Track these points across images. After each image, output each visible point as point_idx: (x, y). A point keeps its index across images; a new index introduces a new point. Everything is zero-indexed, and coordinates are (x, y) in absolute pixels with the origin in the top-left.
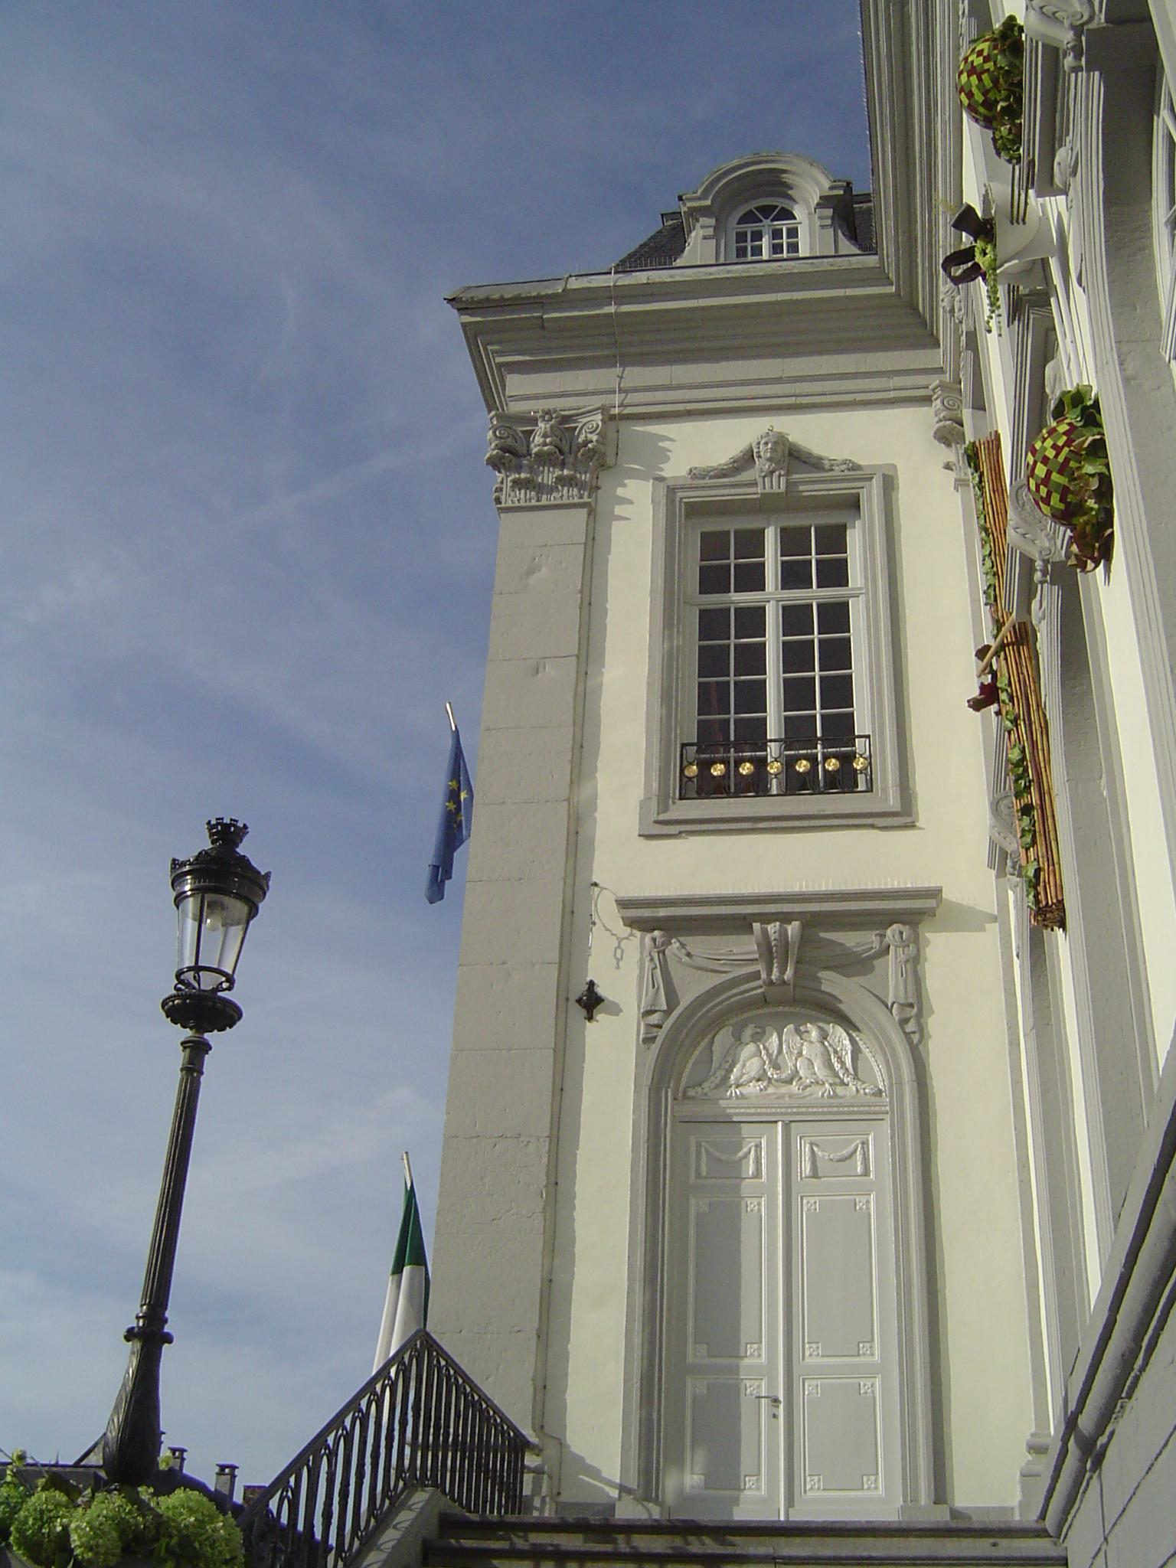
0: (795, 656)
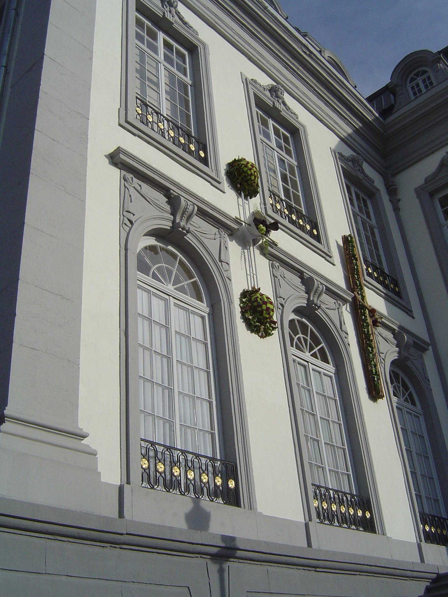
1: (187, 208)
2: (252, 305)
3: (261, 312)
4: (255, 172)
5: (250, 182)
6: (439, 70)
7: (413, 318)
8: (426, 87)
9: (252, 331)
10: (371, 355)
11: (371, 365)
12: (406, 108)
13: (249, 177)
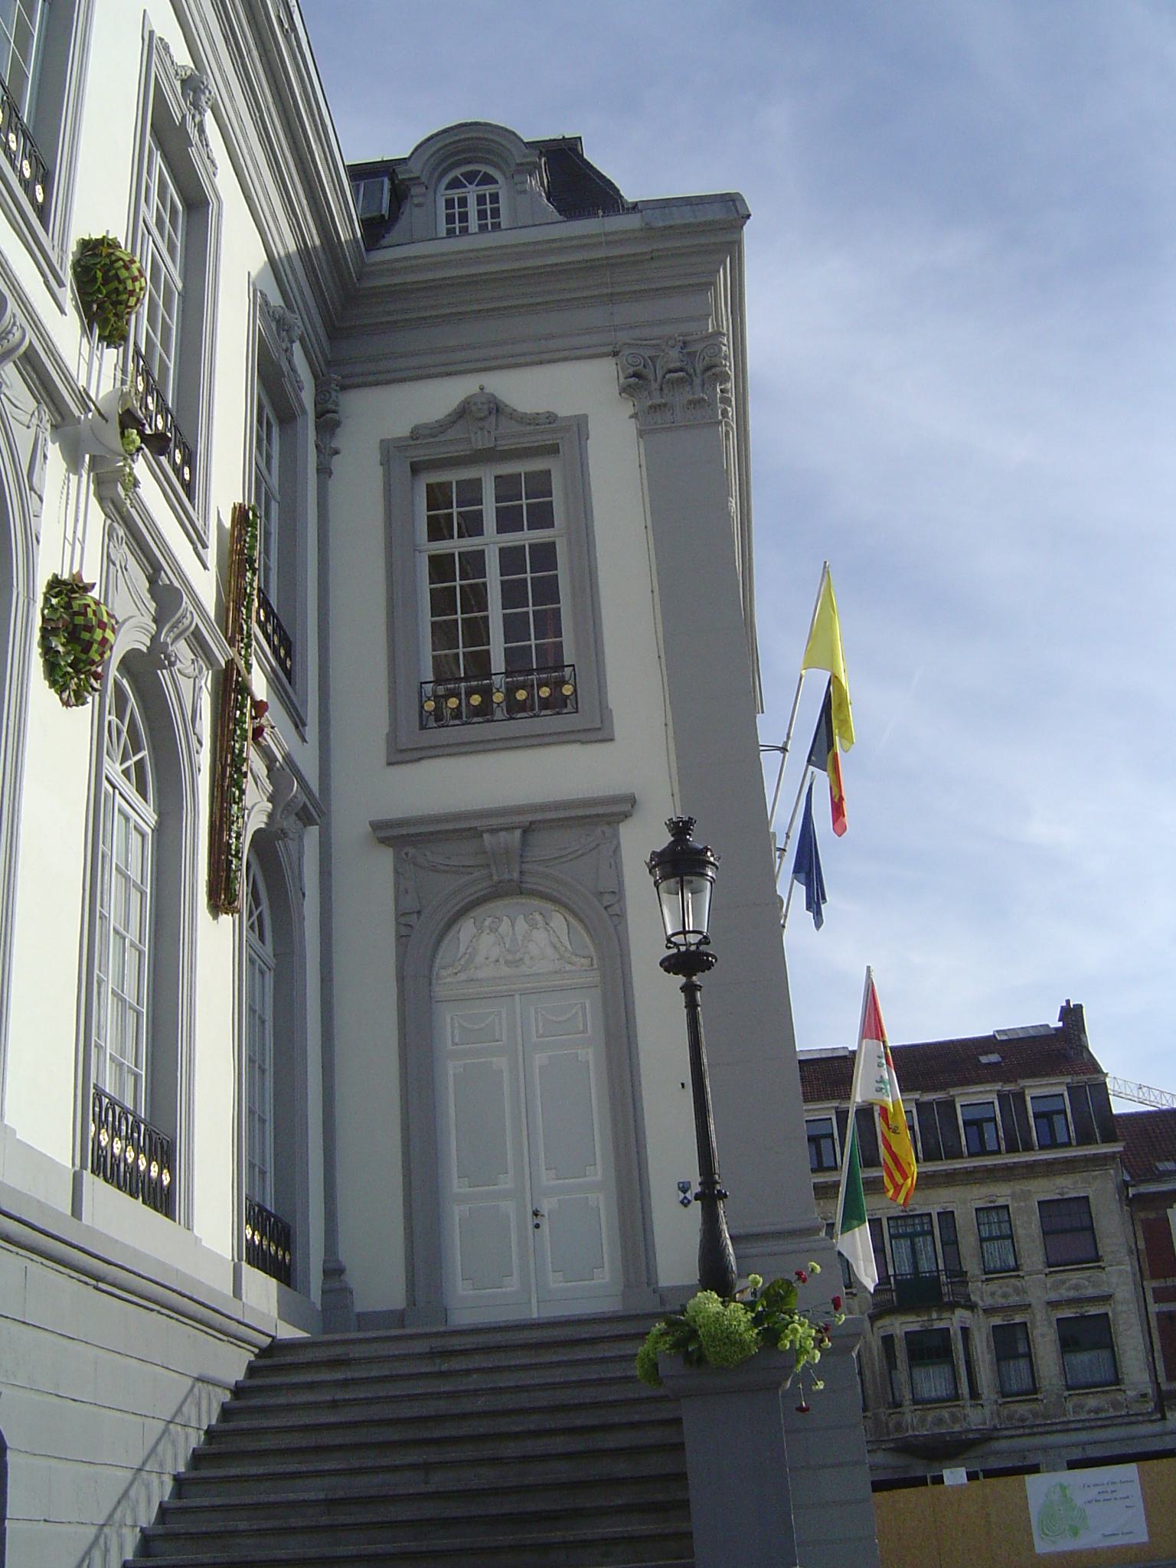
0: (512, 594)
1: (10, 332)
3: (87, 647)
4: (141, 289)
5: (121, 308)
6: (525, 192)
7: (304, 740)
8: (482, 214)
9: (53, 684)
10: (235, 807)
11: (230, 830)
12: (424, 246)
13: (125, 297)
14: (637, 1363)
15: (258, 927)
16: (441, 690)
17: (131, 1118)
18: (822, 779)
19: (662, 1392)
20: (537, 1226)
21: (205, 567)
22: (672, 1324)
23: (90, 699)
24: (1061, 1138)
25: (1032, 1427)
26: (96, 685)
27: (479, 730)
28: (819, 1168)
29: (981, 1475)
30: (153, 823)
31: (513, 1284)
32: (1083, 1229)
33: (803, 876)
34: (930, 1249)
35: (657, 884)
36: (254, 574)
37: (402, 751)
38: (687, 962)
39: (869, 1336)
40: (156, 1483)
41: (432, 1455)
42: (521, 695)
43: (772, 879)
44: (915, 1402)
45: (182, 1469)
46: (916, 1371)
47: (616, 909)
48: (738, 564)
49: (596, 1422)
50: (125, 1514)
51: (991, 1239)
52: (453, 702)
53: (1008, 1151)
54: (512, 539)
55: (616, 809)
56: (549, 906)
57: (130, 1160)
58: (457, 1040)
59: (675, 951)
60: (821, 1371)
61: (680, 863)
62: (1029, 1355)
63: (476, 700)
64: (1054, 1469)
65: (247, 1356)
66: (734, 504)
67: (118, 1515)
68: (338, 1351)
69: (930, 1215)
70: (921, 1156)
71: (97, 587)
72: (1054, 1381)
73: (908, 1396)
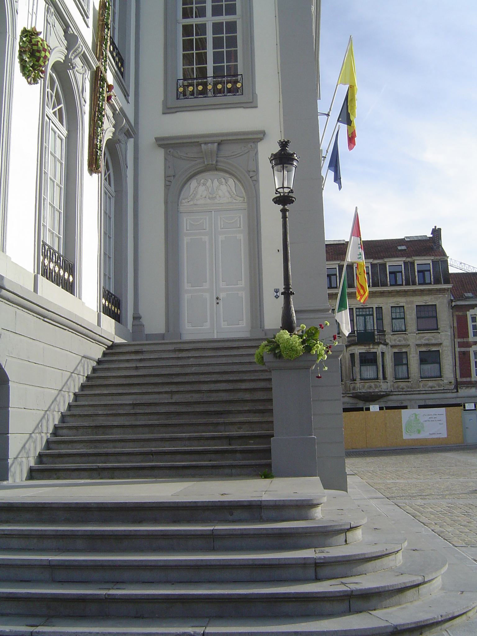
0: (217, 43)
2: (32, 48)
3: (38, 59)
7: (128, 102)
9: (24, 74)
10: (99, 129)
11: (97, 139)
14: (256, 356)
15: (108, 179)
16: (186, 83)
17: (57, 255)
18: (344, 127)
19: (264, 368)
20: (218, 303)
21: (88, 26)
22: (270, 342)
23: (39, 81)
24: (427, 281)
25: (405, 391)
26: (42, 76)
27: (201, 101)
28: (330, 287)
29: (384, 408)
30: (65, 135)
31: (207, 326)
32: (432, 317)
33: (333, 168)
34: (372, 321)
35: (273, 167)
36: (108, 30)
37: (168, 108)
38: (284, 200)
39: (345, 353)
40: (67, 395)
41: (174, 388)
42: (219, 86)
43: (320, 169)
44: (361, 379)
45: (77, 391)
46: (362, 367)
47: (255, 178)
48: (314, 34)
49: (238, 378)
50: (55, 407)
51: (396, 319)
52: (191, 89)
53: (406, 285)
54: (218, 19)
55: (255, 136)
56: (228, 176)
57: (57, 271)
58: (188, 229)
59: (279, 195)
60: (326, 363)
61: (283, 159)
62: (407, 364)
63: (200, 88)
64: (413, 408)
65: (103, 349)
66: (313, 8)
67: (52, 407)
68: (137, 348)
69: (373, 308)
70: (371, 284)
71: (42, 33)
72: (416, 375)
73: (359, 377)
